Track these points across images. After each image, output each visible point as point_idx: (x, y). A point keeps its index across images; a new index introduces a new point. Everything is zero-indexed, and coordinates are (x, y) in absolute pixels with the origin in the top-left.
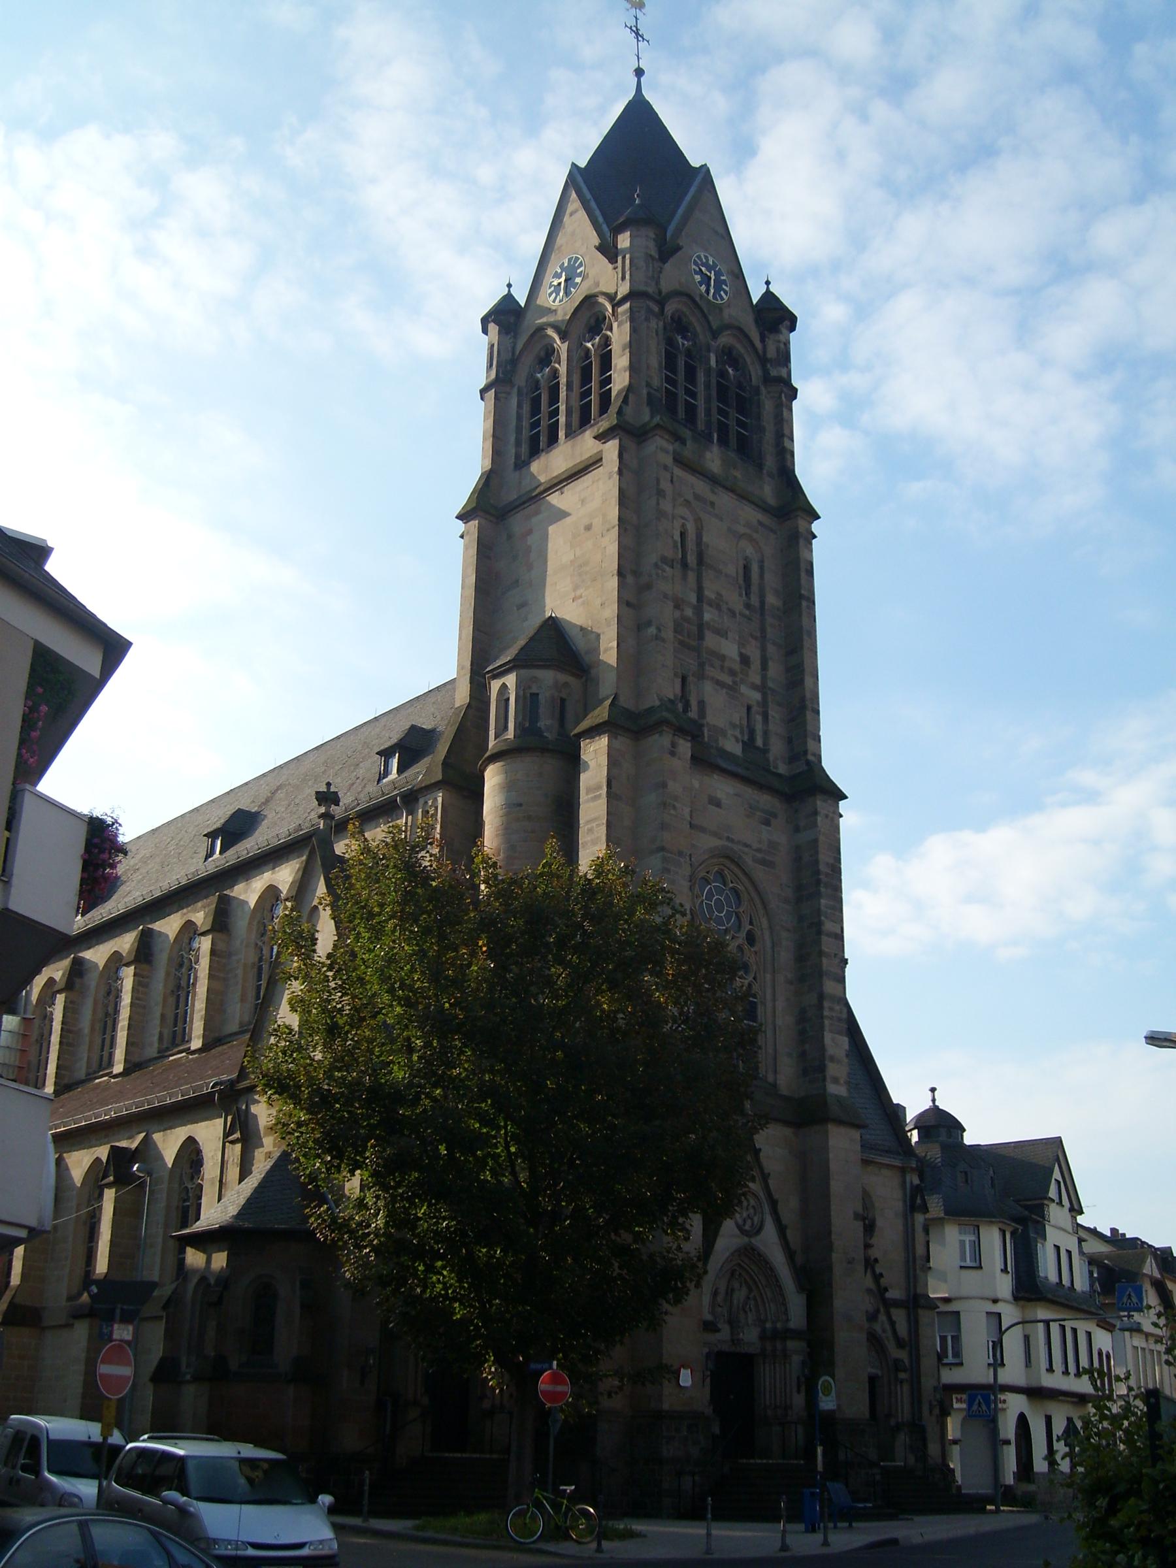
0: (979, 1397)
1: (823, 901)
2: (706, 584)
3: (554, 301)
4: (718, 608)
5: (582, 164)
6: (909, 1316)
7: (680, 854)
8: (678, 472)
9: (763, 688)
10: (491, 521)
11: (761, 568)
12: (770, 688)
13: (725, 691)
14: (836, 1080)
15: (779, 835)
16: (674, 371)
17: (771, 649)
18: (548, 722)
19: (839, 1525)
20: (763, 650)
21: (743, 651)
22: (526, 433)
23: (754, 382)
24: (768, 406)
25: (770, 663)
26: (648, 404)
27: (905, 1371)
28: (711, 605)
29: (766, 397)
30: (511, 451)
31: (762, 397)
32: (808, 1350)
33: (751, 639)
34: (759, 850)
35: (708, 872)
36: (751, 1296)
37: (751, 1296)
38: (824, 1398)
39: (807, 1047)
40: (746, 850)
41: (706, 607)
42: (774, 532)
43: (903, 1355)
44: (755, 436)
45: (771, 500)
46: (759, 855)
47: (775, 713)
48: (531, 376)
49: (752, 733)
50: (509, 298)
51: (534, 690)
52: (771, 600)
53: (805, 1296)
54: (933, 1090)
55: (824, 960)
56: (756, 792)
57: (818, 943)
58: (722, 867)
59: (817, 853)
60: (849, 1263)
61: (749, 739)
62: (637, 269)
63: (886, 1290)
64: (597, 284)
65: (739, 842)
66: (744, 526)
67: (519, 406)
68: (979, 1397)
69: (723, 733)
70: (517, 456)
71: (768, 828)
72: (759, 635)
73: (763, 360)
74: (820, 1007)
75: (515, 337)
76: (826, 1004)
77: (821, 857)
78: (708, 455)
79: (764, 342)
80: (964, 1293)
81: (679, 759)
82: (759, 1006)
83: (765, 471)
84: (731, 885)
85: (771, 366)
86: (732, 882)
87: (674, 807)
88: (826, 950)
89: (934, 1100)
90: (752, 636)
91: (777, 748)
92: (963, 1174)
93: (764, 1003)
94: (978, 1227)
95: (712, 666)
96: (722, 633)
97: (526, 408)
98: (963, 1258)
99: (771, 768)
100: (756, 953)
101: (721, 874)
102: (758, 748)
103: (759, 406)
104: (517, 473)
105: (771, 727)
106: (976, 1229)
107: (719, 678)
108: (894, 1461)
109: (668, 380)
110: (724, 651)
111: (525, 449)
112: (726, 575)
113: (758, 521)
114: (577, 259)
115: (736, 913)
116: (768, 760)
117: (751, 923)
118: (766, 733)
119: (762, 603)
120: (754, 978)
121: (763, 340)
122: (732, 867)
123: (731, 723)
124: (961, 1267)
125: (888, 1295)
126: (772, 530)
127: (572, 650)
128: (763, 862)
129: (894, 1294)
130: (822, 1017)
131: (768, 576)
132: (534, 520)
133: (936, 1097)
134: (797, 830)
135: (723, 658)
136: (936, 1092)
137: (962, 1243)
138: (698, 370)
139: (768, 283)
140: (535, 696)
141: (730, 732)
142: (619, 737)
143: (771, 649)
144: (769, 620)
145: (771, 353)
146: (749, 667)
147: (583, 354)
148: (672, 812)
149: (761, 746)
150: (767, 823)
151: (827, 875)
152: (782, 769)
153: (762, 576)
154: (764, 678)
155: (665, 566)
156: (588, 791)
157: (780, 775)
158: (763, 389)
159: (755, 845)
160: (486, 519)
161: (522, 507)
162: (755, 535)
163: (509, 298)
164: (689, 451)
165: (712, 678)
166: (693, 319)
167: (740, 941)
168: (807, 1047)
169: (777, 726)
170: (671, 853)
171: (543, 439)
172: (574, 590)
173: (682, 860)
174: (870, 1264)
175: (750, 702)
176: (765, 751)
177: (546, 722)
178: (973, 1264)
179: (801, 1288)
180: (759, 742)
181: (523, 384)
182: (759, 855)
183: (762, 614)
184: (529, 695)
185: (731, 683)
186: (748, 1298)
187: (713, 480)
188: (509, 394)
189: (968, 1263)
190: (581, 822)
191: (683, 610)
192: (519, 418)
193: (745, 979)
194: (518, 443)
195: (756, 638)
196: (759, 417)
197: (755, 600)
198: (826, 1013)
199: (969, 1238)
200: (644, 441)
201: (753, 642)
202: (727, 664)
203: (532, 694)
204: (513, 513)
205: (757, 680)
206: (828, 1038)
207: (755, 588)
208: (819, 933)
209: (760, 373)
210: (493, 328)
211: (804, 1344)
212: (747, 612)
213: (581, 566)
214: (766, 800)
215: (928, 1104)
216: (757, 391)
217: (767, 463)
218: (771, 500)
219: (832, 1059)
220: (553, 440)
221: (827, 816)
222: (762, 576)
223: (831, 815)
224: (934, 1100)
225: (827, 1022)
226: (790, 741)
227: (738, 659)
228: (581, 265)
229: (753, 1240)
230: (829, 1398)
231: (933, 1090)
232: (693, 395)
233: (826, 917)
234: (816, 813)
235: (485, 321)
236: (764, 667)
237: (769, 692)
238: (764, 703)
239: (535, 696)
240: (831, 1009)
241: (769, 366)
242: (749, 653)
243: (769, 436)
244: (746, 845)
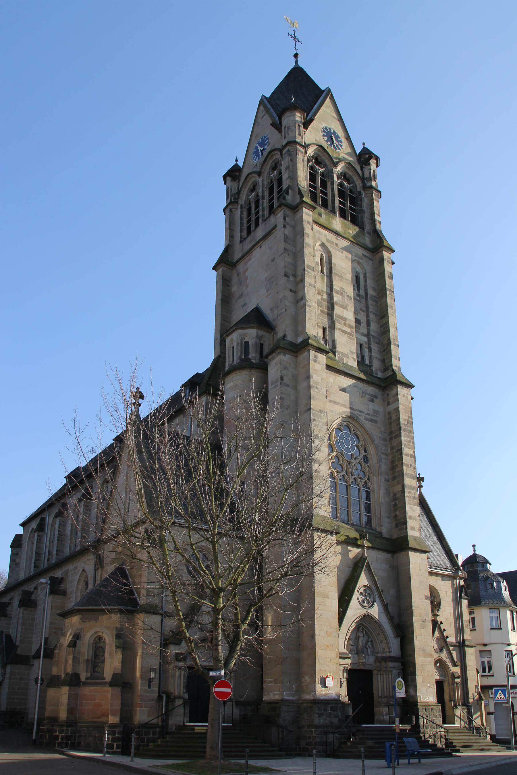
0: (500, 691)
1: (403, 438)
2: (335, 283)
3: (255, 160)
4: (342, 295)
5: (268, 95)
6: (460, 650)
7: (321, 411)
8: (315, 227)
9: (368, 335)
10: (230, 269)
11: (365, 277)
12: (372, 335)
13: (347, 335)
14: (413, 529)
15: (377, 406)
16: (315, 182)
17: (371, 316)
18: (254, 355)
19: (412, 761)
20: (368, 316)
21: (357, 317)
22: (245, 225)
23: (359, 189)
24: (365, 201)
25: (372, 323)
26: (299, 194)
27: (458, 677)
28: (338, 294)
29: (365, 196)
30: (237, 235)
31: (363, 196)
32: (402, 667)
33: (360, 311)
34: (368, 414)
35: (341, 425)
36: (370, 640)
37: (370, 640)
38: (399, 691)
39: (397, 513)
40: (361, 414)
41: (335, 294)
42: (372, 260)
43: (457, 670)
44: (360, 215)
45: (369, 245)
46: (368, 417)
47: (374, 347)
48: (247, 198)
49: (363, 357)
50: (236, 165)
51: (246, 340)
52: (371, 292)
53: (399, 639)
54: (474, 546)
55: (405, 468)
56: (365, 385)
57: (401, 459)
58: (348, 423)
59: (399, 414)
60: (423, 622)
61: (361, 360)
62: (291, 131)
63: (447, 637)
64: (274, 145)
65: (356, 410)
66: (355, 256)
67: (242, 213)
68: (500, 691)
69: (347, 356)
70: (241, 237)
71: (373, 403)
72: (365, 309)
73: (363, 179)
74: (403, 491)
75: (239, 182)
76: (406, 490)
77: (401, 416)
78: (334, 222)
79: (363, 170)
80: (492, 642)
81: (319, 363)
82: (371, 493)
83: (365, 231)
84: (353, 432)
85: (367, 181)
86: (354, 431)
87: (317, 388)
88: (406, 463)
89: (474, 551)
90: (361, 310)
91: (376, 365)
92: (491, 584)
93: (373, 491)
94: (499, 609)
95: (339, 323)
96: (345, 307)
97: (245, 214)
98: (492, 624)
99: (374, 374)
100: (369, 466)
101: (347, 426)
102: (367, 365)
103: (361, 200)
104: (241, 244)
105: (373, 354)
106: (498, 610)
107: (343, 329)
108: (455, 724)
109: (311, 186)
110: (345, 316)
111: (245, 233)
112: (346, 279)
113: (363, 254)
114: (265, 137)
115: (357, 447)
116: (372, 370)
117: (365, 451)
118: (370, 357)
119: (366, 294)
120: (368, 479)
121: (362, 169)
122: (353, 423)
123: (351, 351)
124: (491, 629)
125: (448, 640)
126: (370, 259)
127: (266, 320)
128: (371, 420)
129: (452, 639)
130: (404, 496)
131: (368, 281)
132: (249, 263)
133: (476, 550)
134: (389, 404)
135: (345, 319)
136: (476, 548)
137: (491, 617)
138: (328, 183)
139: (364, 144)
140: (247, 343)
141: (350, 356)
142: (287, 355)
143: (371, 316)
144: (370, 302)
145: (366, 175)
146: (360, 325)
147: (269, 181)
148: (316, 390)
149: (368, 364)
150: (372, 401)
151: (405, 425)
152: (380, 375)
153: (365, 281)
154: (369, 330)
155: (309, 270)
156: (272, 384)
157: (379, 378)
158: (363, 192)
159: (366, 412)
160: (227, 267)
161: (243, 259)
162: (361, 261)
163: (236, 165)
164: (323, 220)
165: (340, 329)
166: (324, 158)
167: (359, 460)
168: (397, 513)
169: (375, 354)
170: (316, 411)
171: (253, 226)
172: (267, 291)
173: (322, 415)
174: (435, 624)
175: (362, 342)
176: (371, 366)
177: (253, 355)
178: (497, 627)
179: (397, 636)
180: (367, 362)
181: (243, 203)
182: (368, 417)
183: (366, 298)
184: (244, 343)
185: (350, 332)
186: (368, 641)
187: (337, 234)
188: (237, 208)
189: (494, 627)
190: (269, 400)
191: (322, 296)
192: (242, 219)
193: (363, 479)
194: (241, 231)
195: (363, 311)
196: (361, 206)
197: (362, 293)
198: (406, 494)
199: (494, 615)
200: (297, 211)
201: (362, 313)
202: (347, 322)
203: (245, 342)
204: (239, 263)
205: (365, 332)
206: (408, 507)
207: (362, 287)
208: (401, 454)
209: (361, 185)
210: (228, 179)
211: (400, 664)
212: (358, 298)
213: (270, 279)
214: (371, 389)
215: (472, 553)
216: (360, 194)
217: (367, 228)
218: (369, 245)
219: (411, 517)
220: (257, 224)
221: (404, 396)
222: (365, 281)
223: (406, 395)
224: (474, 551)
225: (407, 499)
226: (384, 361)
227: (354, 320)
228: (267, 139)
229: (369, 611)
230: (401, 691)
231: (474, 546)
232: (326, 194)
233: (405, 446)
234: (397, 394)
235: (225, 177)
236: (368, 324)
237: (371, 337)
238: (369, 343)
239: (247, 343)
240: (409, 492)
241: (366, 181)
242: (360, 318)
243: (367, 215)
244: (360, 412)
